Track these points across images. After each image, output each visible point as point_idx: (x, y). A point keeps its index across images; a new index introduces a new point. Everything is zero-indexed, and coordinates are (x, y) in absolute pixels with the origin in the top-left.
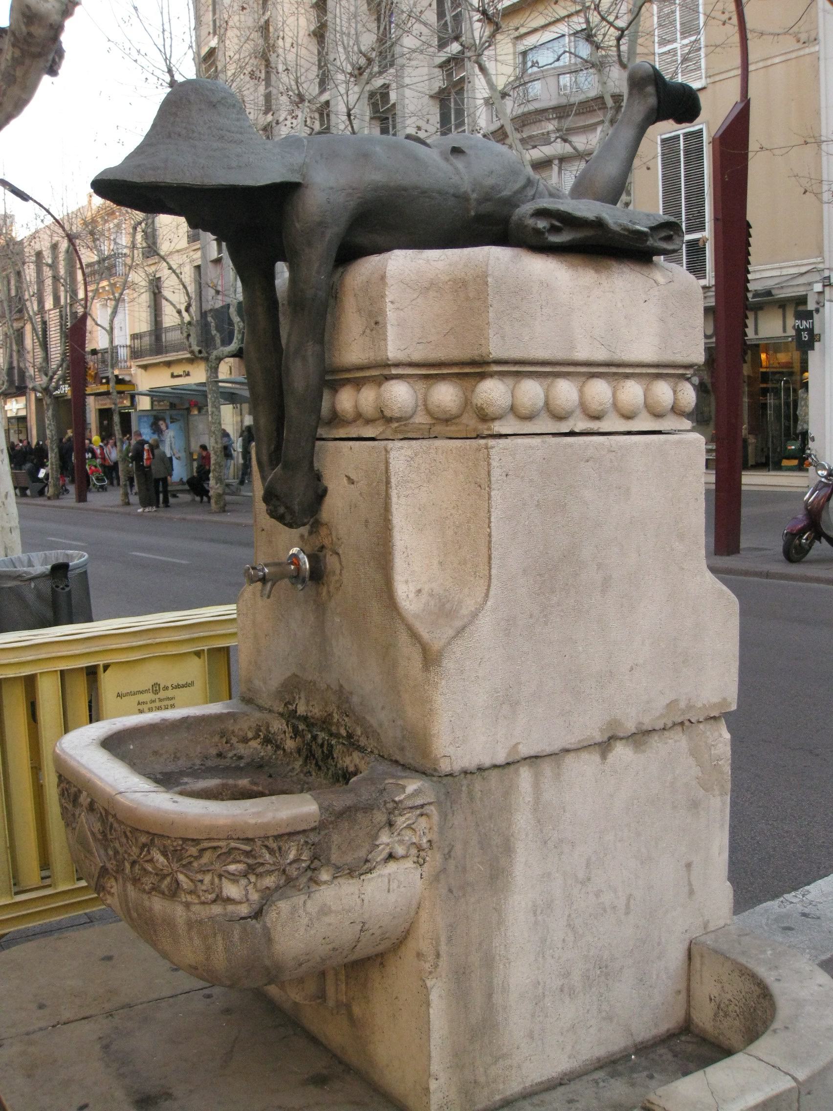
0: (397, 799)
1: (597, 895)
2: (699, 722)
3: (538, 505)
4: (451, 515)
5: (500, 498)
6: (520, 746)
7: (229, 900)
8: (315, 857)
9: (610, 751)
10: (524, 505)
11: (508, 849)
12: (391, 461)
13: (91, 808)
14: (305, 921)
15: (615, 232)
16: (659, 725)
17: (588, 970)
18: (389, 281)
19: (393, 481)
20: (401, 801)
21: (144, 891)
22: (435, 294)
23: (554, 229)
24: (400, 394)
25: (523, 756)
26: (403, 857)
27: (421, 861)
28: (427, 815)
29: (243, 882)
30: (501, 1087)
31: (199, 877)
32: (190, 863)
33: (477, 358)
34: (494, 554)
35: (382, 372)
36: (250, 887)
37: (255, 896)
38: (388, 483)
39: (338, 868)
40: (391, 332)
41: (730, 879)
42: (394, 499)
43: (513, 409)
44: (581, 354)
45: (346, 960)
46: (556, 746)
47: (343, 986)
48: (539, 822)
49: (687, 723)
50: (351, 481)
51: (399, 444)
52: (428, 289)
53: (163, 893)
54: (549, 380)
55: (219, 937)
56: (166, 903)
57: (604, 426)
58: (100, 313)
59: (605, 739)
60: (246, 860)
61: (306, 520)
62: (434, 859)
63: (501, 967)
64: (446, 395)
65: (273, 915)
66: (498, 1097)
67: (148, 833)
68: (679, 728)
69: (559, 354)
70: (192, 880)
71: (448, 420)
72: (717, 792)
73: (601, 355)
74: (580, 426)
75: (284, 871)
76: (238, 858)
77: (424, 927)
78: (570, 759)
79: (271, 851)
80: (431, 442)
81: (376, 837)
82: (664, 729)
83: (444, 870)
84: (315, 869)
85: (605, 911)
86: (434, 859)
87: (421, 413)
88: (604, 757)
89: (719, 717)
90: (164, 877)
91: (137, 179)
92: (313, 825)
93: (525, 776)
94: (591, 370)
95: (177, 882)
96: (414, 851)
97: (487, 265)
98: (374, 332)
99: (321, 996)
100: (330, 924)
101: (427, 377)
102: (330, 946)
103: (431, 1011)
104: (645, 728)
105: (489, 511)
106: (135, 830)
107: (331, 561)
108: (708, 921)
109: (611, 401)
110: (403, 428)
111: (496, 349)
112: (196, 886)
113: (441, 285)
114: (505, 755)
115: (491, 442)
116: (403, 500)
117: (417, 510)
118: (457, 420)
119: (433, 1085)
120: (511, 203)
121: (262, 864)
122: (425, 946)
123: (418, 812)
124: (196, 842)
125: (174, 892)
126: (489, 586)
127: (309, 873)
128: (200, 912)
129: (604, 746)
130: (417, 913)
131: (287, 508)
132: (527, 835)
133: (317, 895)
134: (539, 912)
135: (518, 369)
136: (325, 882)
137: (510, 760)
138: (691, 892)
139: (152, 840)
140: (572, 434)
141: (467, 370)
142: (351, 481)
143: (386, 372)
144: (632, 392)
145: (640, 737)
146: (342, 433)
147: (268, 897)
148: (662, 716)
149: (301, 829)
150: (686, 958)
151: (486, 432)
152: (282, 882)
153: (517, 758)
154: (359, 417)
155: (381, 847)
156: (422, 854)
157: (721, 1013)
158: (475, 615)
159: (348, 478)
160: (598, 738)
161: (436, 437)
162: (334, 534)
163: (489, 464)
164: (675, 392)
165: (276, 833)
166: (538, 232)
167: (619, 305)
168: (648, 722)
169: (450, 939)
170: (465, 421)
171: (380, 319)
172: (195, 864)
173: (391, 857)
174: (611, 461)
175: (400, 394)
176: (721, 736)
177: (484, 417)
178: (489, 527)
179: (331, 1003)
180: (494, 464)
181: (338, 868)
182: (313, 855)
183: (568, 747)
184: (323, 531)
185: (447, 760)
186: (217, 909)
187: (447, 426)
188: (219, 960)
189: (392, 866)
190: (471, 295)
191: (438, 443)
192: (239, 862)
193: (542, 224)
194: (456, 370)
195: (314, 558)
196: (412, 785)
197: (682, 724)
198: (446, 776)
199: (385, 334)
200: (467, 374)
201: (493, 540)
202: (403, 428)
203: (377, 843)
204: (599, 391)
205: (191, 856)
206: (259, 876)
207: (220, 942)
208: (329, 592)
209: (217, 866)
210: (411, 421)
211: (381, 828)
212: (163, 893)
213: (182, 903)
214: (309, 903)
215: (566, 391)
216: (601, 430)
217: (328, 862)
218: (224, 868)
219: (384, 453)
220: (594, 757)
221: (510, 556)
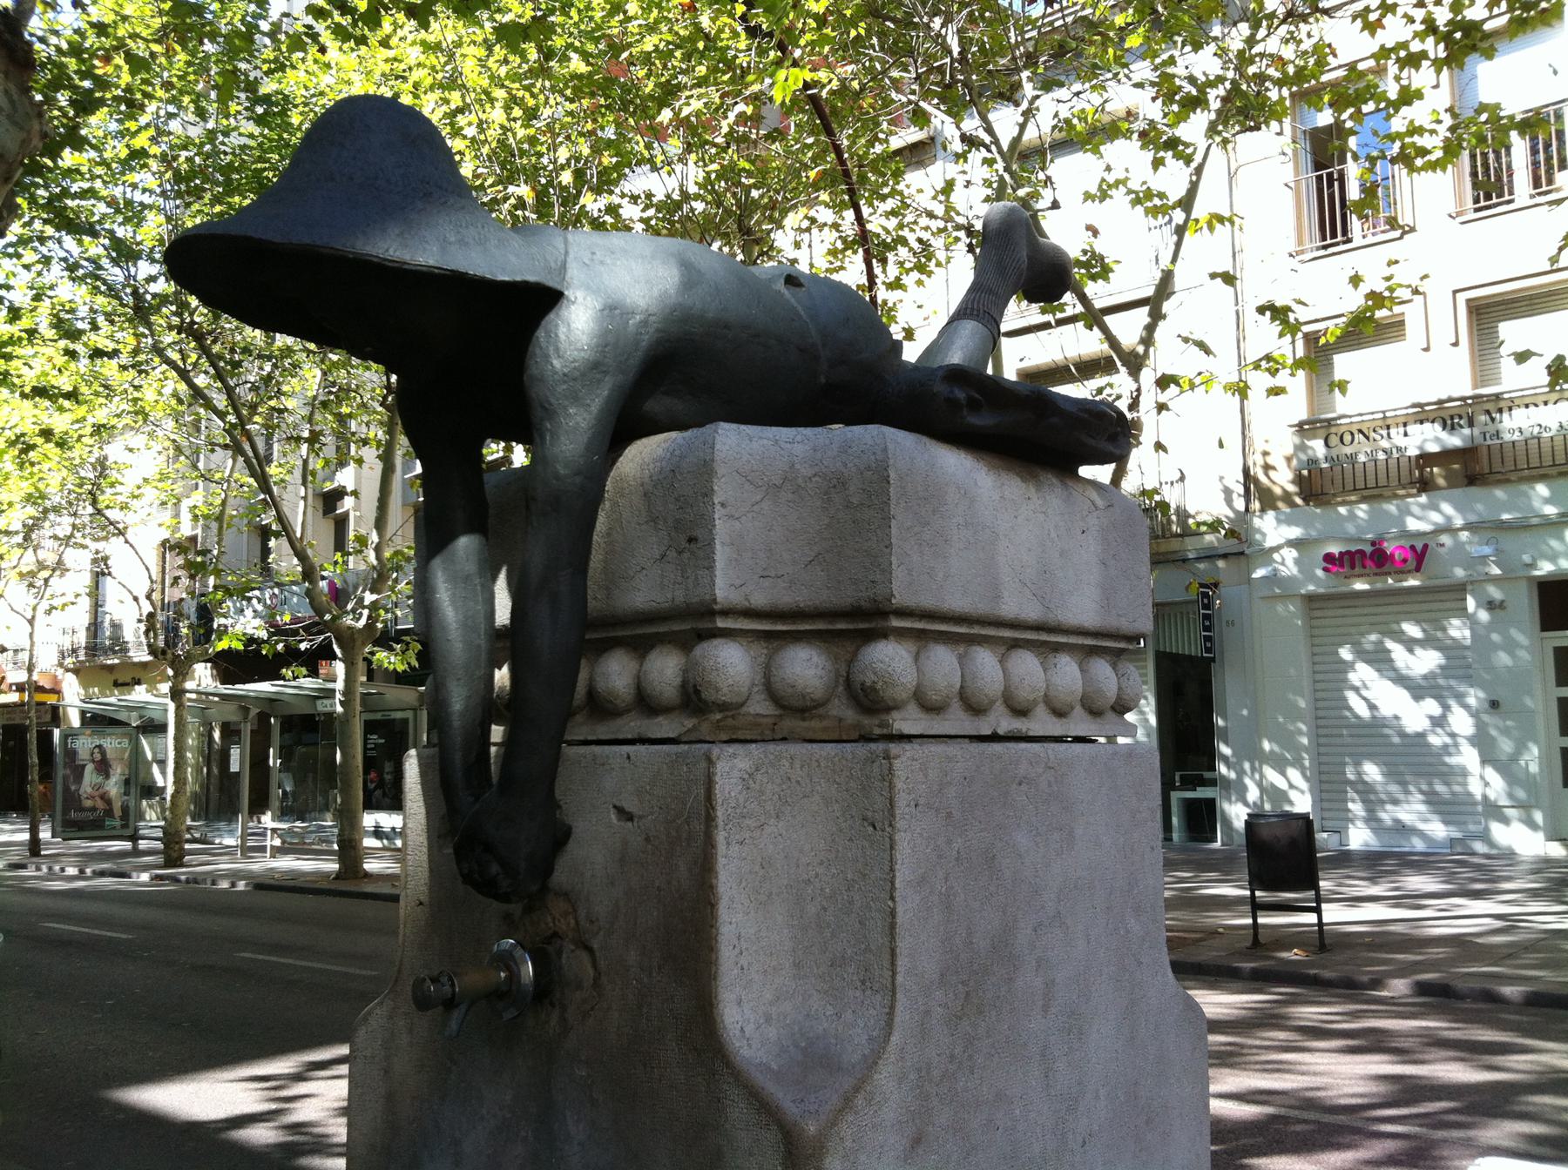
4: (817, 875)
5: (912, 844)
10: (940, 857)
12: (717, 778)
18: (721, 470)
19: (720, 813)
22: (791, 496)
23: (974, 405)
24: (731, 664)
34: (903, 945)
35: (696, 623)
38: (710, 819)
40: (721, 555)
42: (721, 848)
50: (625, 815)
64: (805, 667)
69: (981, 607)
73: (1032, 613)
74: (1006, 724)
80: (781, 747)
87: (758, 697)
98: (686, 555)
101: (768, 636)
105: (892, 870)
107: (574, 963)
110: (730, 721)
111: (902, 595)
113: (800, 481)
115: (894, 748)
117: (757, 868)
118: (821, 711)
126: (892, 1007)
140: (995, 738)
143: (704, 625)
146: (603, 731)
151: (877, 731)
158: (872, 1063)
159: (620, 811)
161: (784, 739)
162: (582, 913)
163: (891, 786)
167: (1053, 535)
170: (834, 712)
171: (698, 533)
175: (731, 664)
178: (892, 898)
180: (899, 785)
187: (804, 719)
190: (855, 501)
194: (820, 626)
200: (840, 633)
201: (899, 920)
202: (730, 721)
204: (1026, 666)
210: (744, 709)
216: (1031, 734)
219: (703, 764)
221: (919, 953)
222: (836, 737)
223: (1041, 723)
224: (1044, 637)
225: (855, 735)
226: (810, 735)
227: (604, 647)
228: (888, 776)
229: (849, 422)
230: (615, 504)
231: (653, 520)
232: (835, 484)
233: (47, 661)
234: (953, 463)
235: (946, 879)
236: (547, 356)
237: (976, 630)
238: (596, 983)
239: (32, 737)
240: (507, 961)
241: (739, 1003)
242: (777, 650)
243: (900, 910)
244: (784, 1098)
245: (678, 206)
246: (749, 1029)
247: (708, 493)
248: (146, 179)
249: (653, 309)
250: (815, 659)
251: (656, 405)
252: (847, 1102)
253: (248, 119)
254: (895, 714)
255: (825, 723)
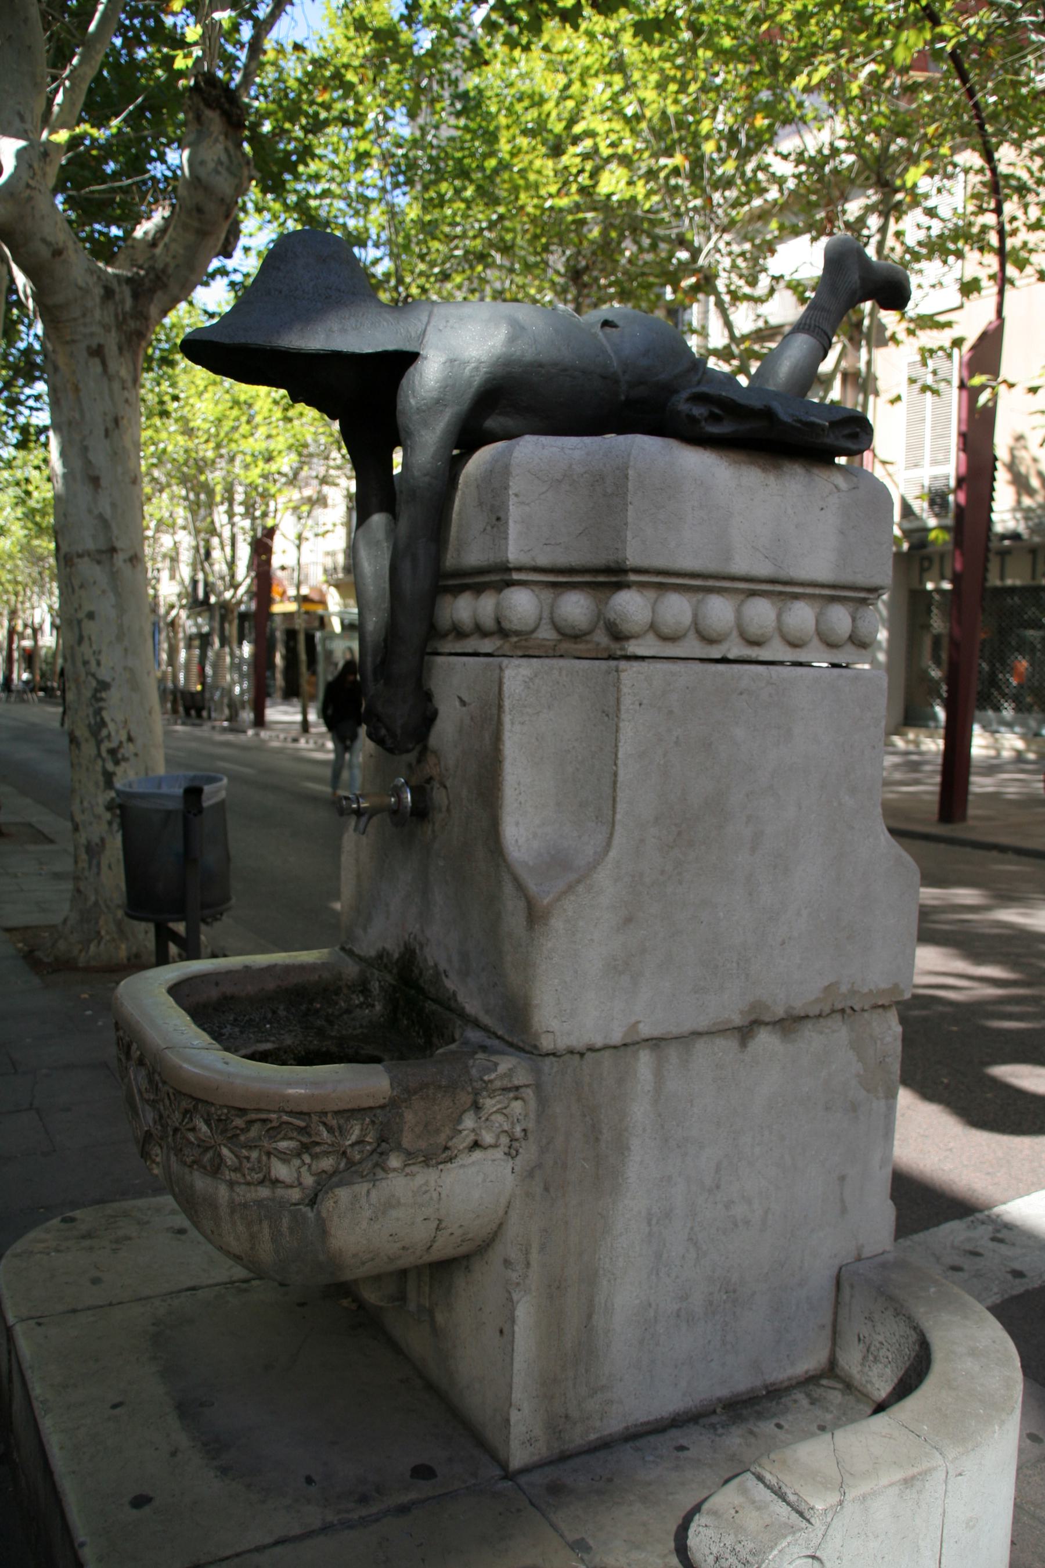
0: (486, 1078)
1: (727, 1207)
2: (863, 1010)
3: (677, 743)
6: (641, 1026)
7: (276, 1182)
8: (382, 1139)
9: (752, 1037)
11: (622, 1148)
12: (505, 680)
13: (141, 1062)
14: (368, 1213)
15: (784, 424)
16: (814, 1011)
17: (711, 1294)
18: (515, 471)
19: (507, 704)
20: (491, 1081)
21: (185, 1163)
23: (714, 418)
24: (522, 604)
25: (643, 1036)
26: (491, 1146)
27: (514, 1153)
28: (522, 1099)
29: (297, 1162)
30: (598, 1424)
31: (245, 1152)
32: (237, 1136)
33: (612, 565)
34: (620, 795)
35: (499, 577)
36: (304, 1169)
37: (309, 1180)
38: (500, 707)
39: (409, 1154)
40: (513, 529)
41: (893, 1197)
43: (653, 627)
44: (740, 566)
45: (421, 1262)
46: (687, 1027)
47: (427, 1289)
48: (660, 1115)
49: (848, 1011)
50: (463, 703)
51: (516, 661)
52: (559, 481)
53: (204, 1168)
54: (700, 596)
55: (265, 1224)
56: (209, 1180)
57: (764, 654)
58: (287, 526)
59: (746, 1024)
60: (300, 1138)
61: (411, 746)
62: (529, 1152)
63: (605, 1283)
64: (575, 607)
65: (329, 1204)
66: (592, 1437)
67: (191, 1097)
68: (838, 1017)
70: (236, 1156)
71: (577, 636)
72: (881, 1095)
73: (764, 569)
75: (344, 1153)
76: (290, 1134)
77: (513, 1229)
78: (701, 1046)
79: (330, 1130)
81: (459, 1120)
82: (820, 1016)
83: (540, 1166)
84: (382, 1154)
85: (736, 1225)
86: (529, 1152)
88: (743, 1043)
89: (890, 1006)
90: (207, 1149)
91: (227, 341)
92: (382, 1102)
93: (645, 1059)
94: (751, 587)
95: (220, 1155)
96: (504, 1140)
97: (629, 455)
99: (402, 1298)
100: (398, 1219)
101: (554, 585)
102: (399, 1245)
103: (516, 1328)
104: (796, 1013)
105: (616, 746)
106: (178, 1093)
107: (439, 796)
108: (863, 1246)
109: (774, 624)
110: (523, 643)
111: (633, 557)
112: (241, 1163)
114: (620, 1035)
115: (623, 664)
116: (517, 728)
118: (588, 638)
119: (514, 1416)
120: (669, 389)
121: (318, 1144)
122: (514, 1254)
123: (511, 1095)
124: (242, 1111)
125: (215, 1169)
126: (612, 834)
127: (375, 1157)
128: (243, 1194)
129: (745, 1032)
130: (506, 1213)
131: (388, 730)
132: (644, 1130)
133: (384, 1183)
134: (654, 1222)
135: (664, 580)
136: (395, 1170)
137: (628, 1041)
138: (844, 1211)
139: (195, 1107)
140: (724, 660)
141: (601, 579)
142: (463, 703)
143: (506, 577)
144: (802, 616)
145: (790, 1023)
146: (458, 647)
147: (326, 1183)
148: (817, 1000)
149: (365, 1105)
150: (834, 1289)
151: (619, 653)
152: (342, 1165)
153: (636, 1038)
154: (480, 631)
155: (465, 1133)
156: (516, 1144)
157: (871, 1358)
158: (593, 866)
159: (460, 698)
160: (737, 1020)
161: (561, 656)
163: (619, 690)
164: (854, 620)
165: (336, 1108)
166: (693, 420)
168: (799, 1006)
169: (542, 1248)
171: (501, 515)
172: (242, 1138)
173: (476, 1145)
174: (770, 695)
175: (522, 604)
176: (890, 1028)
177: (618, 635)
179: (412, 1306)
180: (625, 690)
181: (409, 1154)
182: (379, 1140)
183: (700, 1029)
184: (431, 759)
185: (550, 1036)
186: (264, 1192)
188: (266, 1251)
189: (478, 1155)
190: (609, 491)
191: (562, 662)
192: (291, 1139)
193: (699, 411)
195: (419, 792)
196: (505, 1064)
197: (843, 1011)
198: (548, 1055)
199: (506, 532)
202: (523, 643)
203: (460, 1128)
204: (761, 613)
205: (236, 1127)
206: (315, 1157)
207: (266, 1231)
208: (433, 831)
209: (265, 1143)
210: (535, 635)
211: (464, 1111)
212: (204, 1168)
213: (226, 1181)
214: (374, 1193)
215: (720, 610)
216: (761, 659)
217: (399, 1147)
218: (274, 1145)
219: (498, 671)
220: (727, 1046)
221: (637, 798)
222: (594, 655)
223: (776, 650)
224: (781, 589)
225: (606, 655)
226: (578, 654)
227: (458, 590)
228: (617, 684)
229: (620, 432)
230: (463, 493)
231: (481, 504)
232: (598, 479)
233: (316, 577)
234: (695, 461)
235: (665, 755)
236: (407, 396)
237: (710, 583)
238: (448, 810)
239: (302, 638)
240: (397, 792)
241: (517, 824)
242: (560, 594)
243: (621, 773)
244: (532, 886)
245: (826, 159)
246: (521, 841)
247: (506, 488)
248: (370, 175)
249: (484, 358)
250: (582, 601)
251: (491, 423)
252: (570, 888)
253: (451, 114)
254: (632, 642)
255: (589, 646)
